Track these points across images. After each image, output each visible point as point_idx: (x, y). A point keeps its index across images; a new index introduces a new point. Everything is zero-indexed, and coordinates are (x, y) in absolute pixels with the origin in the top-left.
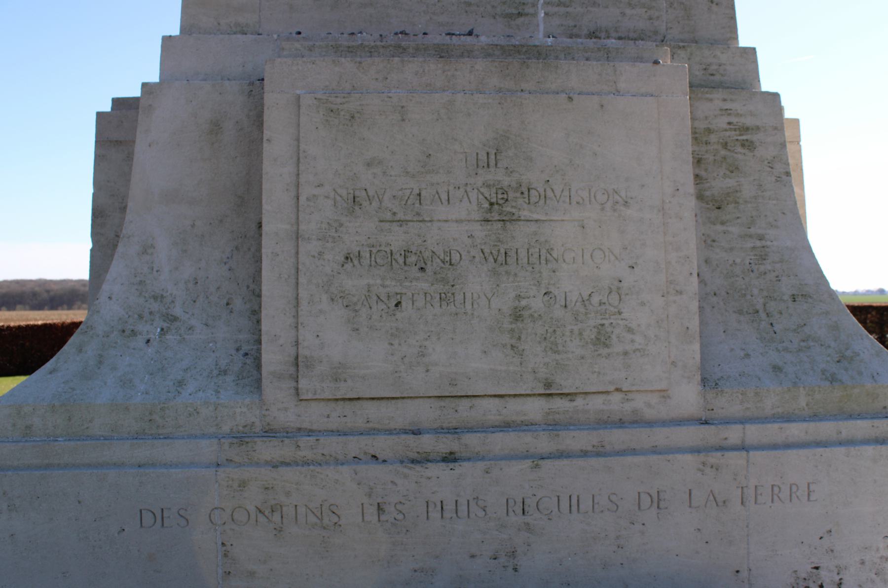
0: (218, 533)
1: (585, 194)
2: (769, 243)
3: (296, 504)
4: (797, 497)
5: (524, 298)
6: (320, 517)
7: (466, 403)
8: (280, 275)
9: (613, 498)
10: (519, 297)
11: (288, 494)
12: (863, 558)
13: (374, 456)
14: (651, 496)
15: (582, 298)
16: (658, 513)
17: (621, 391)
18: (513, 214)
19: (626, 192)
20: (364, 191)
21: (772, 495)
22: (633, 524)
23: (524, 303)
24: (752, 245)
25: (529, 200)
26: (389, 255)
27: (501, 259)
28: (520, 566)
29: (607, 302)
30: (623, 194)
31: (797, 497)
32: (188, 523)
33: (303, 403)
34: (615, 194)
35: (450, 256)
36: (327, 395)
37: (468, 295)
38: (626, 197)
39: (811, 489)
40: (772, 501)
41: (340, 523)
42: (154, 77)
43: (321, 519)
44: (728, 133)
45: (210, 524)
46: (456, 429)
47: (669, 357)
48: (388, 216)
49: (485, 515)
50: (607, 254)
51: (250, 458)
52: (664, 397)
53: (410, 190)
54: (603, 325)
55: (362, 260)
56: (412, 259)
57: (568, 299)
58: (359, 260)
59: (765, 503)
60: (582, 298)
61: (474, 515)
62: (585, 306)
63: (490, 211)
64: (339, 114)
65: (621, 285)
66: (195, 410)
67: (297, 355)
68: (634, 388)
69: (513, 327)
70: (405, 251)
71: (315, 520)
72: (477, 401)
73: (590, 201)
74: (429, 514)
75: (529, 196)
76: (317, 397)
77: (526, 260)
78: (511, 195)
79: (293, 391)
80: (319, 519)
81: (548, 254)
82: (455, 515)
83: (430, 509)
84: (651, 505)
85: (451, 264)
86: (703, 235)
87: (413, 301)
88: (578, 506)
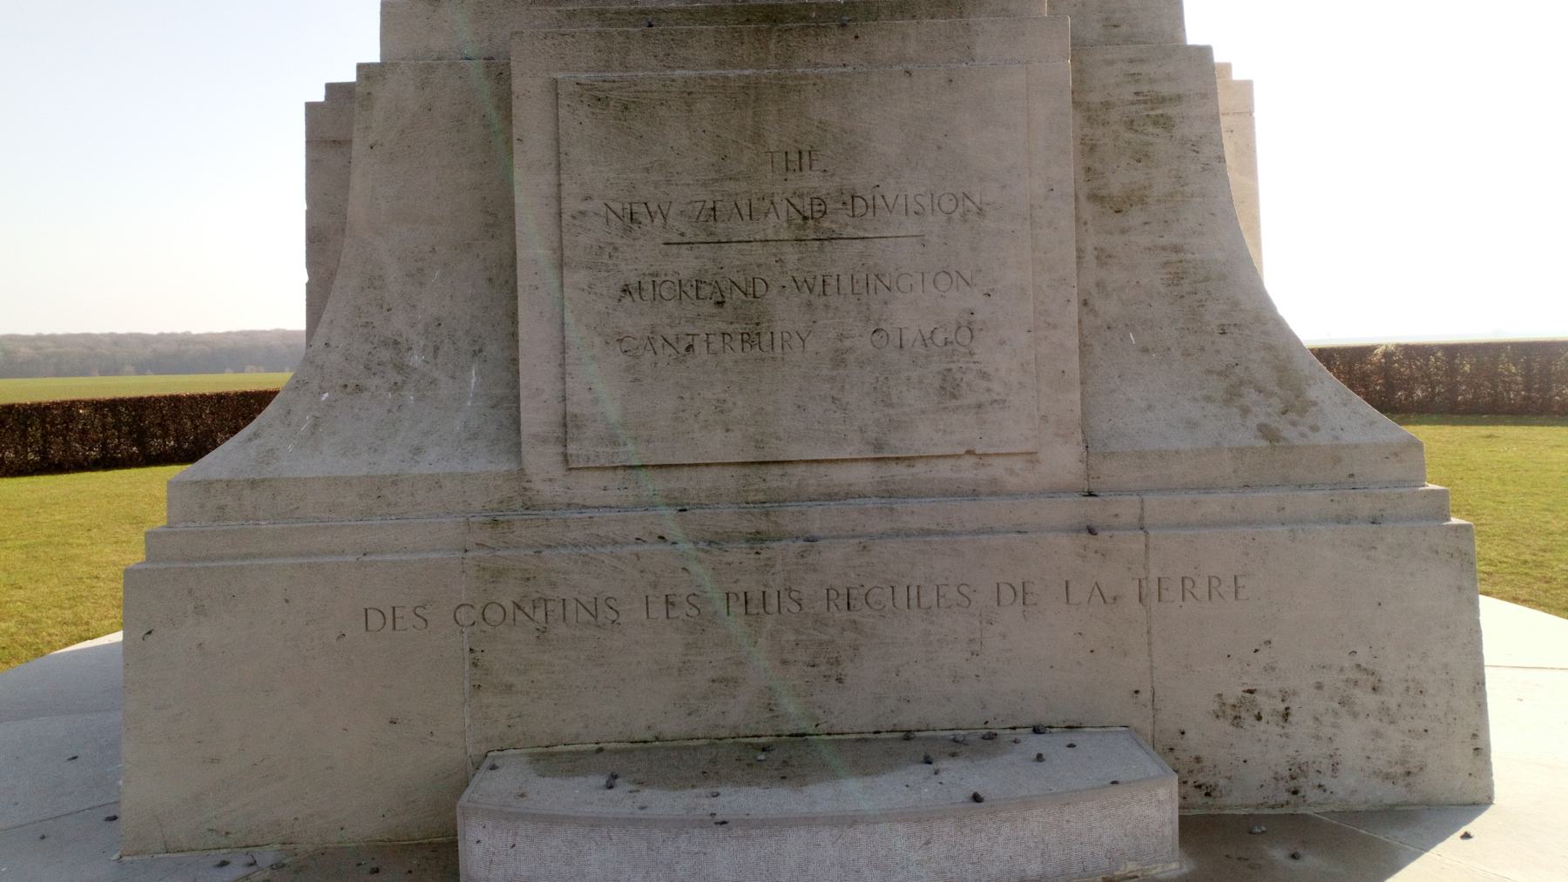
0: (466, 636)
1: (926, 201)
2: (1189, 256)
3: (564, 597)
4: (1220, 594)
5: (847, 338)
6: (594, 614)
7: (776, 470)
8: (541, 313)
9: (963, 589)
10: (841, 337)
11: (553, 585)
12: (1319, 680)
13: (662, 538)
14: (1013, 588)
15: (923, 337)
16: (1024, 611)
17: (974, 454)
18: (833, 231)
19: (981, 196)
20: (644, 205)
21: (1183, 591)
22: (991, 624)
23: (847, 343)
24: (1165, 260)
25: (853, 211)
26: (678, 288)
27: (818, 289)
28: (846, 675)
29: (955, 341)
30: (977, 199)
31: (1220, 594)
32: (427, 624)
33: (574, 473)
34: (966, 200)
35: (754, 287)
36: (603, 462)
37: (777, 336)
38: (981, 203)
39: (1239, 584)
40: (1183, 599)
41: (620, 620)
42: (373, 56)
43: (596, 617)
44: (1134, 108)
45: (456, 625)
46: (765, 503)
47: (1038, 409)
48: (676, 238)
49: (801, 610)
50: (955, 279)
51: (506, 540)
52: (1032, 461)
53: (702, 204)
54: (950, 370)
55: (643, 294)
56: (706, 290)
57: (904, 338)
58: (640, 294)
59: (1172, 601)
60: (923, 337)
61: (786, 610)
62: (926, 346)
63: (802, 227)
64: (608, 105)
65: (973, 318)
66: (436, 483)
67: (565, 413)
68: (991, 451)
69: (834, 374)
70: (697, 281)
71: (588, 617)
72: (789, 469)
73: (933, 210)
74: (730, 609)
75: (853, 208)
76: (591, 464)
77: (849, 291)
78: (831, 206)
79: (560, 458)
80: (592, 615)
81: (878, 281)
82: (762, 611)
83: (731, 603)
84: (1015, 600)
85: (755, 297)
86: (1095, 249)
87: (708, 343)
88: (919, 599)
